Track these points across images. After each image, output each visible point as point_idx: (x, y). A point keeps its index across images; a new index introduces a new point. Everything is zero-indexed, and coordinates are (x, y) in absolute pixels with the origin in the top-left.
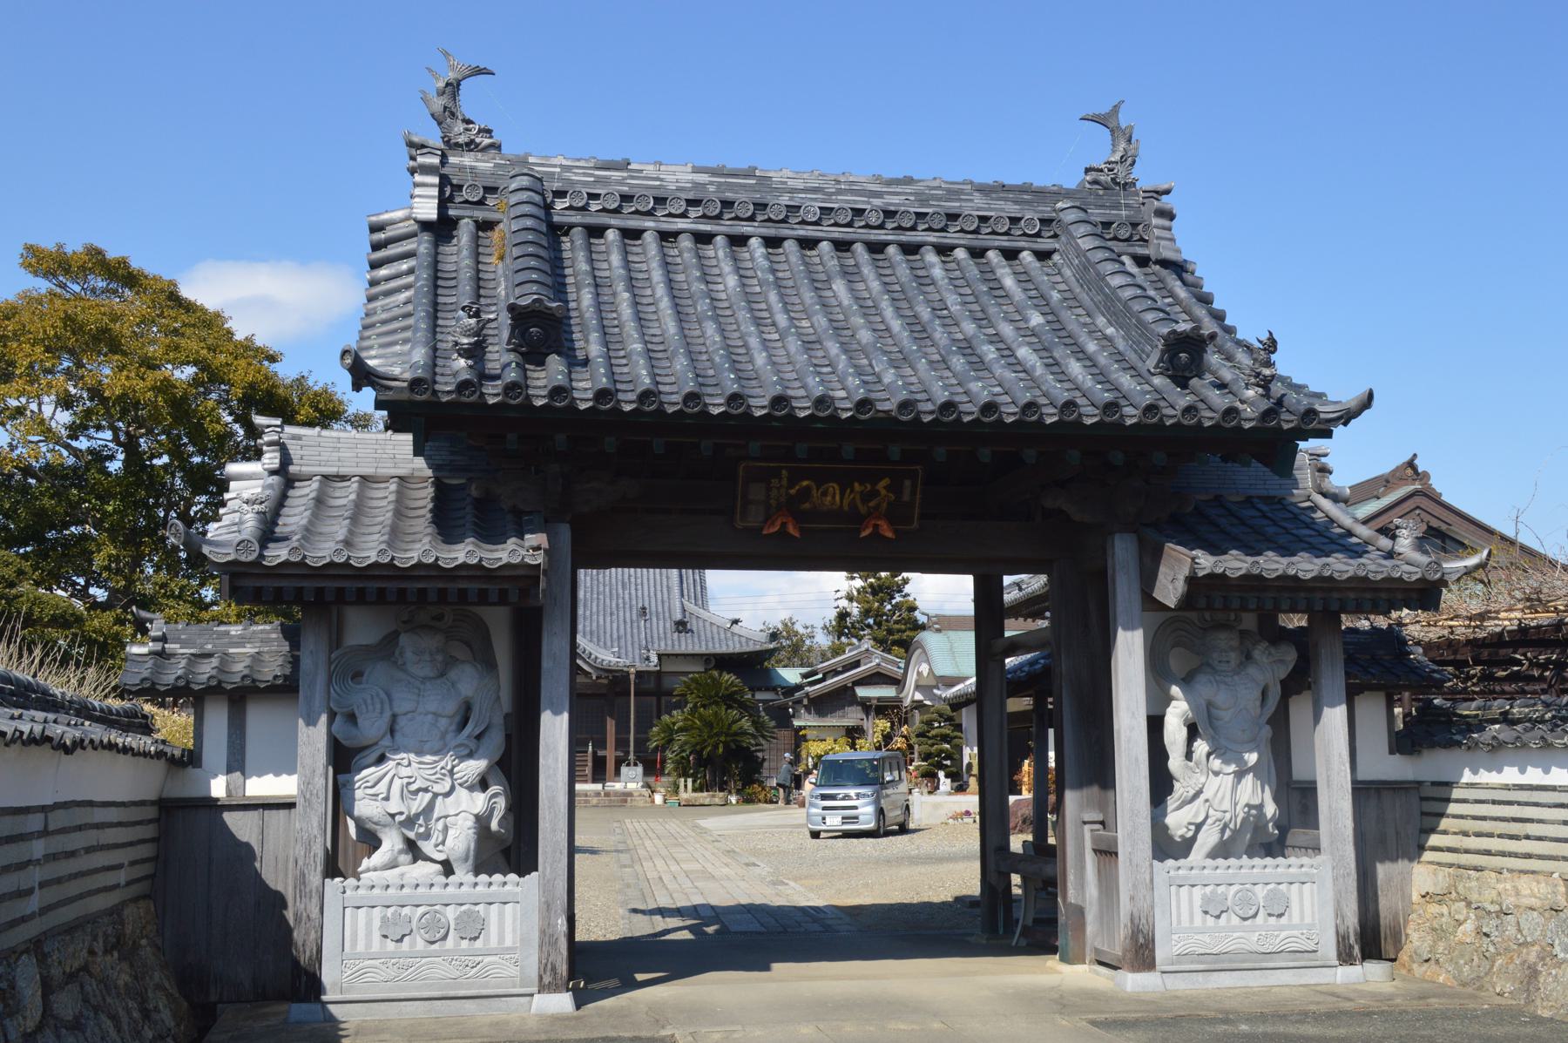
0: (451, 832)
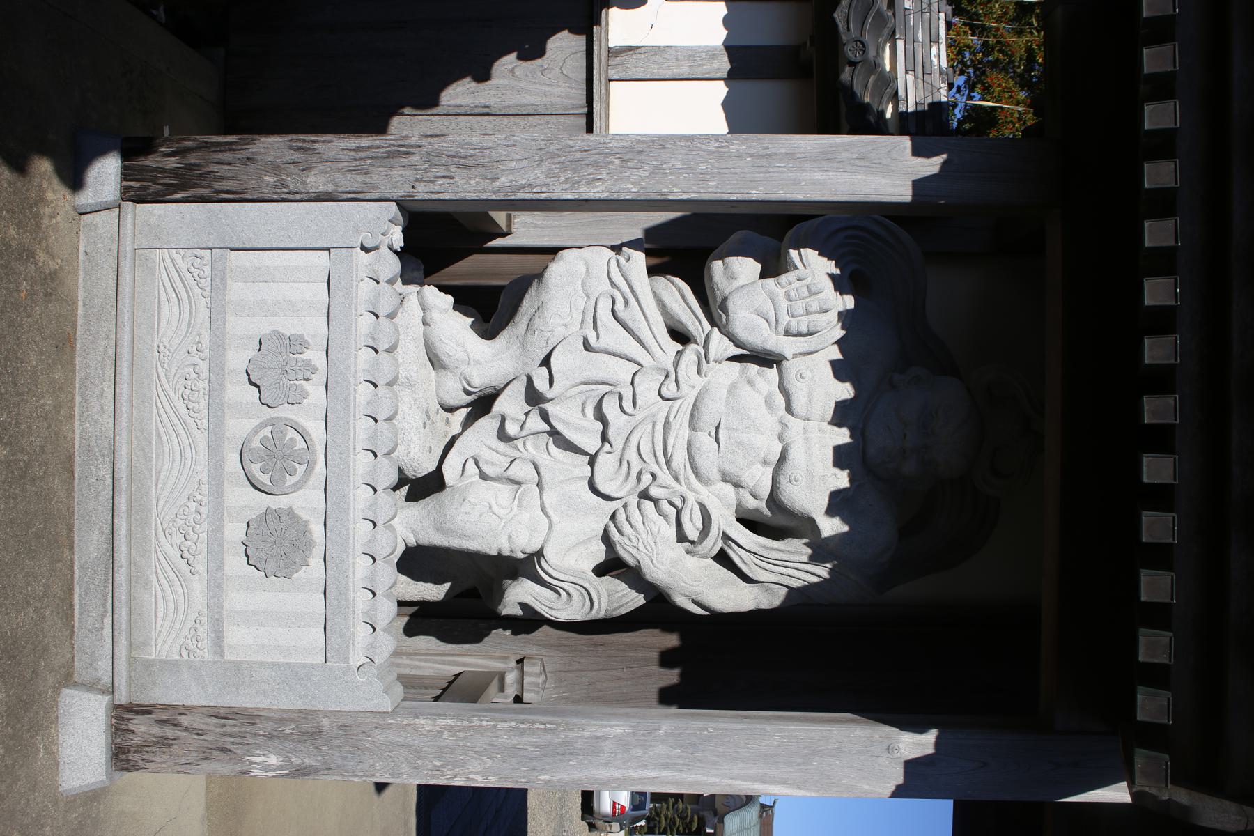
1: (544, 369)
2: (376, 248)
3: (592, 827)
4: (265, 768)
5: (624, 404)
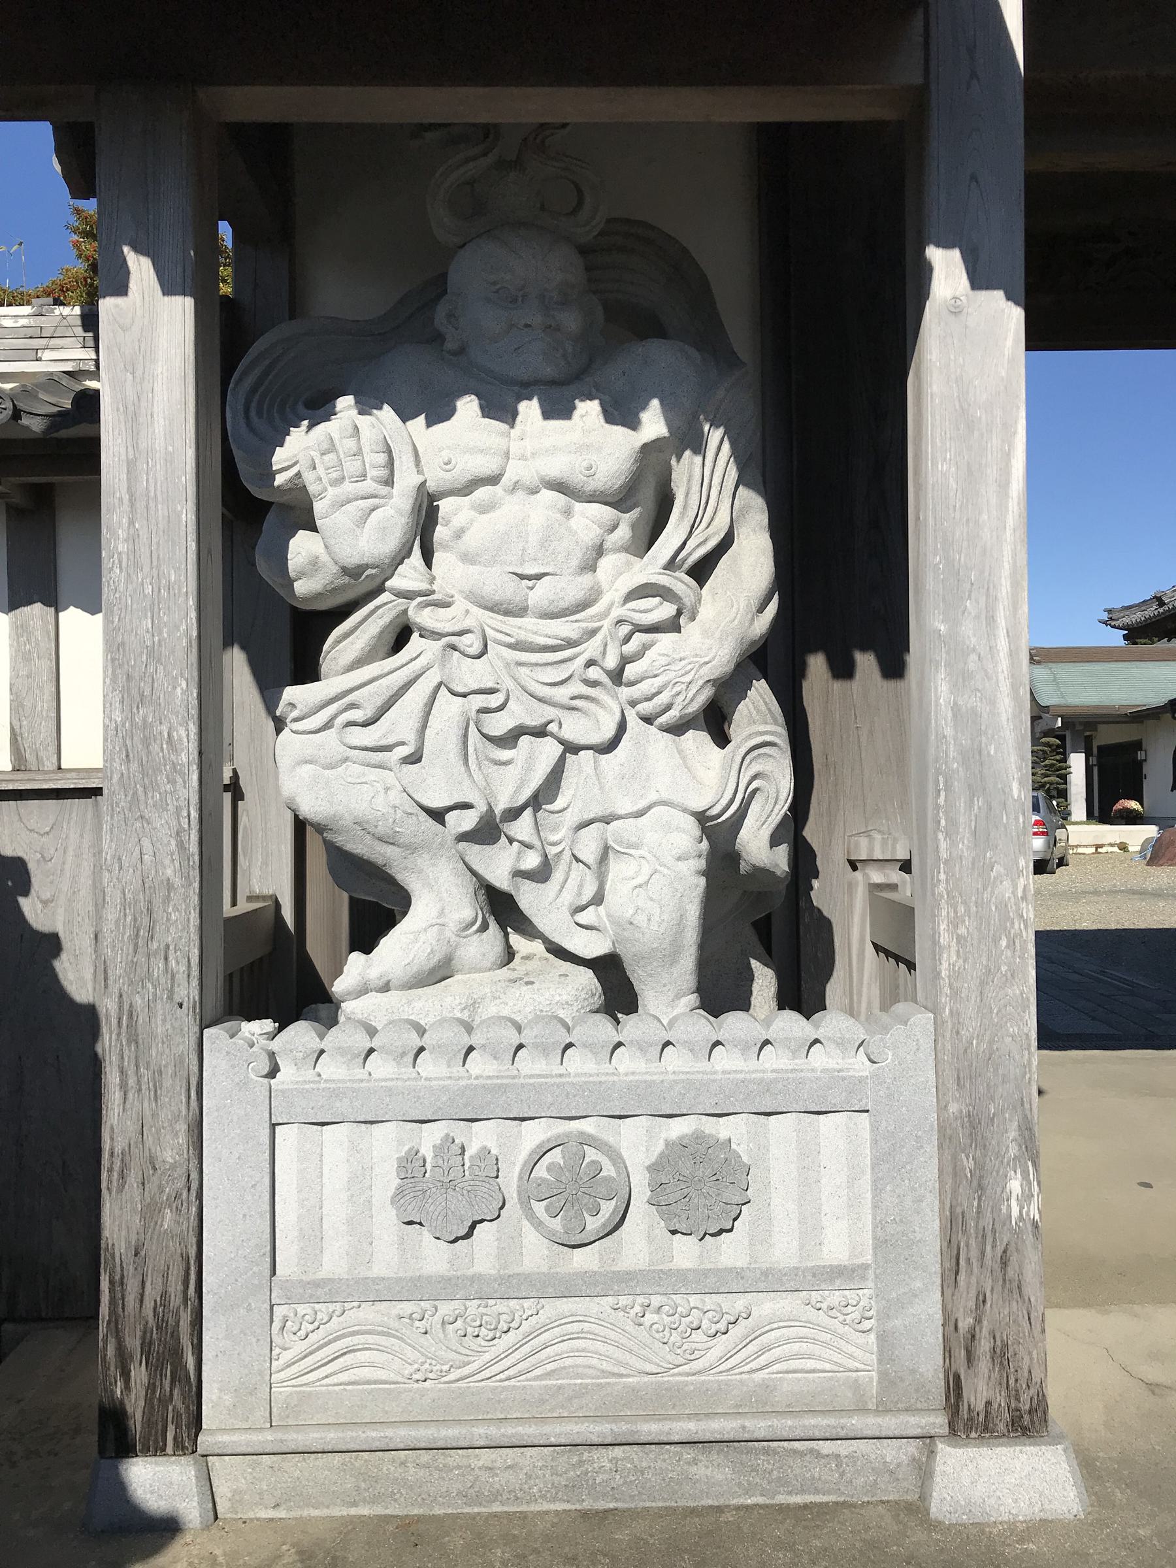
0: (617, 869)
1: (450, 817)
2: (272, 1055)
3: (1062, 862)
4: (1026, 1197)
5: (494, 705)
